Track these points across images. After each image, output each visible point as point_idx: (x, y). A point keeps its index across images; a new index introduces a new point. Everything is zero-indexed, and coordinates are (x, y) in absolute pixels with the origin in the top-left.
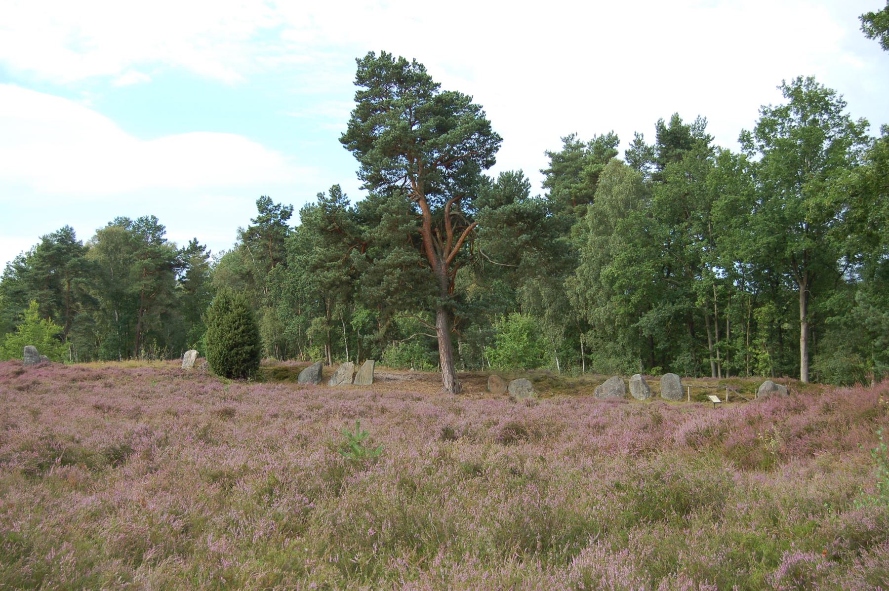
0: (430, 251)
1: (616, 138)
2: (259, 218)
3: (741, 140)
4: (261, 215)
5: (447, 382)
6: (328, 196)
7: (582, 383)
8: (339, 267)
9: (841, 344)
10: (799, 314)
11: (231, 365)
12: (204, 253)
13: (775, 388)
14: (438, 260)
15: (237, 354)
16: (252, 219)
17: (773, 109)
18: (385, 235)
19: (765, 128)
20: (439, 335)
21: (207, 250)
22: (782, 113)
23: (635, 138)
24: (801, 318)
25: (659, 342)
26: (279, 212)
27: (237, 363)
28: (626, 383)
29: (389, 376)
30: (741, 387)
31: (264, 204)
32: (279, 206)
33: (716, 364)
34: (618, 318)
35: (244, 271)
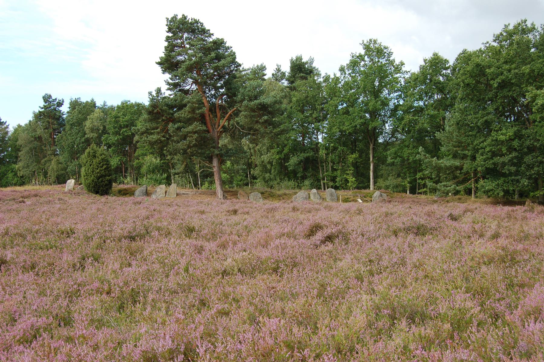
0: (209, 125)
1: (265, 67)
2: (45, 106)
3: (340, 70)
4: (45, 104)
5: (220, 195)
6: (154, 94)
7: (285, 194)
8: (158, 133)
9: (391, 173)
10: (370, 159)
11: (99, 188)
12: (5, 125)
13: (381, 195)
14: (213, 130)
15: (102, 181)
16: (40, 107)
17: (358, 55)
18: (188, 115)
19: (354, 64)
20: (215, 170)
21: (7, 124)
22: (361, 57)
23: (277, 67)
24: (371, 161)
25: (298, 173)
26: (56, 103)
27: (102, 186)
28: (309, 194)
29: (183, 192)
30: (364, 195)
31: (47, 98)
32: (56, 99)
33: (324, 184)
34: (275, 161)
35: (37, 136)
